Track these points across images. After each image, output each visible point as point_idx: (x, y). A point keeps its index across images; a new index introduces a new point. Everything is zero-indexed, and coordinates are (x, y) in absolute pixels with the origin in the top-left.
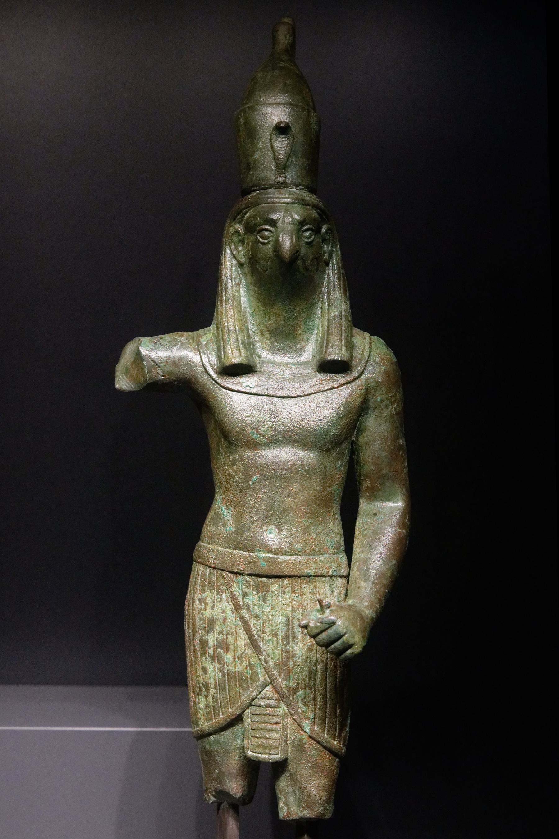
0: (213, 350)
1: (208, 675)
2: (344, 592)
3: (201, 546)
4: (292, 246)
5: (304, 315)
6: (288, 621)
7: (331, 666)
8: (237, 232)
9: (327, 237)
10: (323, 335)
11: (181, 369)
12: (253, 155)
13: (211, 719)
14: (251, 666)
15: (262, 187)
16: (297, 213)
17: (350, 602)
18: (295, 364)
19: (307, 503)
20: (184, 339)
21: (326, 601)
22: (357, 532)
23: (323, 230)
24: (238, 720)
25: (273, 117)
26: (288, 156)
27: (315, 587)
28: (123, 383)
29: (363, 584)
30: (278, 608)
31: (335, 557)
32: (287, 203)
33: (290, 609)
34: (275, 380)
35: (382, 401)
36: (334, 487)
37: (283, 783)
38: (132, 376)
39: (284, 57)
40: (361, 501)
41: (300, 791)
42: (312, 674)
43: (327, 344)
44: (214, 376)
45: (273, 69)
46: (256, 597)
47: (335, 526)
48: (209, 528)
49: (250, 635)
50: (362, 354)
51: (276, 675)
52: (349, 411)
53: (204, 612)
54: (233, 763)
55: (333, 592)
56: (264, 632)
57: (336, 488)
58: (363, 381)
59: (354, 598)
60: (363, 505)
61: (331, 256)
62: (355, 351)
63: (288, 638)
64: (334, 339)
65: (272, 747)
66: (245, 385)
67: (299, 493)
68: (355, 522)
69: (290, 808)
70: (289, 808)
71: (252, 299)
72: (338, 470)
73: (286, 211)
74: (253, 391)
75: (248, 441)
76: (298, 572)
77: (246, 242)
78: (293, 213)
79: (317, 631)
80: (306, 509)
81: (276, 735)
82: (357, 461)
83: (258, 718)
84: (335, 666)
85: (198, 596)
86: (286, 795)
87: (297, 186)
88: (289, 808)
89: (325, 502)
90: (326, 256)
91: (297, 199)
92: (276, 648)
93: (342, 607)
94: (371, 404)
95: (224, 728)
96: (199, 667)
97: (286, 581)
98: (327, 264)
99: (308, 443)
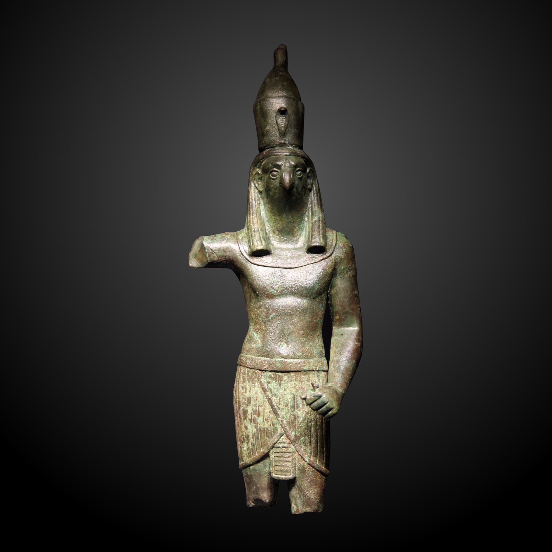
0: (246, 242)
1: (248, 431)
2: (325, 380)
3: (242, 356)
4: (291, 180)
5: (298, 220)
6: (294, 397)
7: (319, 422)
8: (258, 173)
9: (310, 175)
10: (309, 232)
11: (228, 254)
12: (265, 128)
13: (251, 457)
14: (273, 424)
15: (272, 146)
16: (293, 161)
17: (330, 385)
18: (293, 249)
19: (303, 329)
20: (228, 237)
21: (315, 385)
22: (332, 345)
23: (308, 171)
24: (266, 456)
25: (277, 105)
26: (286, 127)
27: (309, 377)
28: (194, 263)
29: (337, 374)
30: (288, 390)
31: (320, 359)
32: (286, 155)
33: (295, 390)
34: (283, 258)
35: (344, 269)
36: (318, 319)
37: (294, 492)
38: (199, 259)
39: (282, 69)
40: (334, 328)
41: (304, 497)
42: (309, 428)
43: (312, 237)
44: (247, 257)
45: (276, 76)
46: (275, 384)
47: (319, 342)
48: (247, 345)
49: (272, 406)
50: (332, 243)
51: (288, 429)
52: (326, 275)
53: (245, 394)
54: (264, 482)
55: (319, 379)
56: (280, 404)
57: (319, 320)
58: (333, 258)
59: (332, 382)
60: (335, 330)
61: (312, 186)
62: (328, 240)
63: (294, 407)
64: (316, 234)
65: (287, 471)
66: (265, 262)
67: (297, 323)
68: (330, 340)
69: (298, 506)
70: (297, 507)
71: (267, 212)
72: (320, 309)
73: (286, 159)
74: (270, 265)
75: (268, 294)
76: (298, 369)
77: (263, 178)
78: (290, 161)
79: (311, 401)
80: (302, 332)
81: (289, 464)
82: (331, 305)
83: (278, 455)
84: (322, 423)
85: (241, 385)
86: (295, 499)
87: (292, 145)
88: (297, 507)
89: (311, 329)
90: (309, 186)
91: (292, 152)
92: (287, 413)
93: (325, 387)
94: (338, 271)
95: (258, 461)
96: (243, 426)
97: (292, 374)
98: (310, 191)
99: (302, 294)
